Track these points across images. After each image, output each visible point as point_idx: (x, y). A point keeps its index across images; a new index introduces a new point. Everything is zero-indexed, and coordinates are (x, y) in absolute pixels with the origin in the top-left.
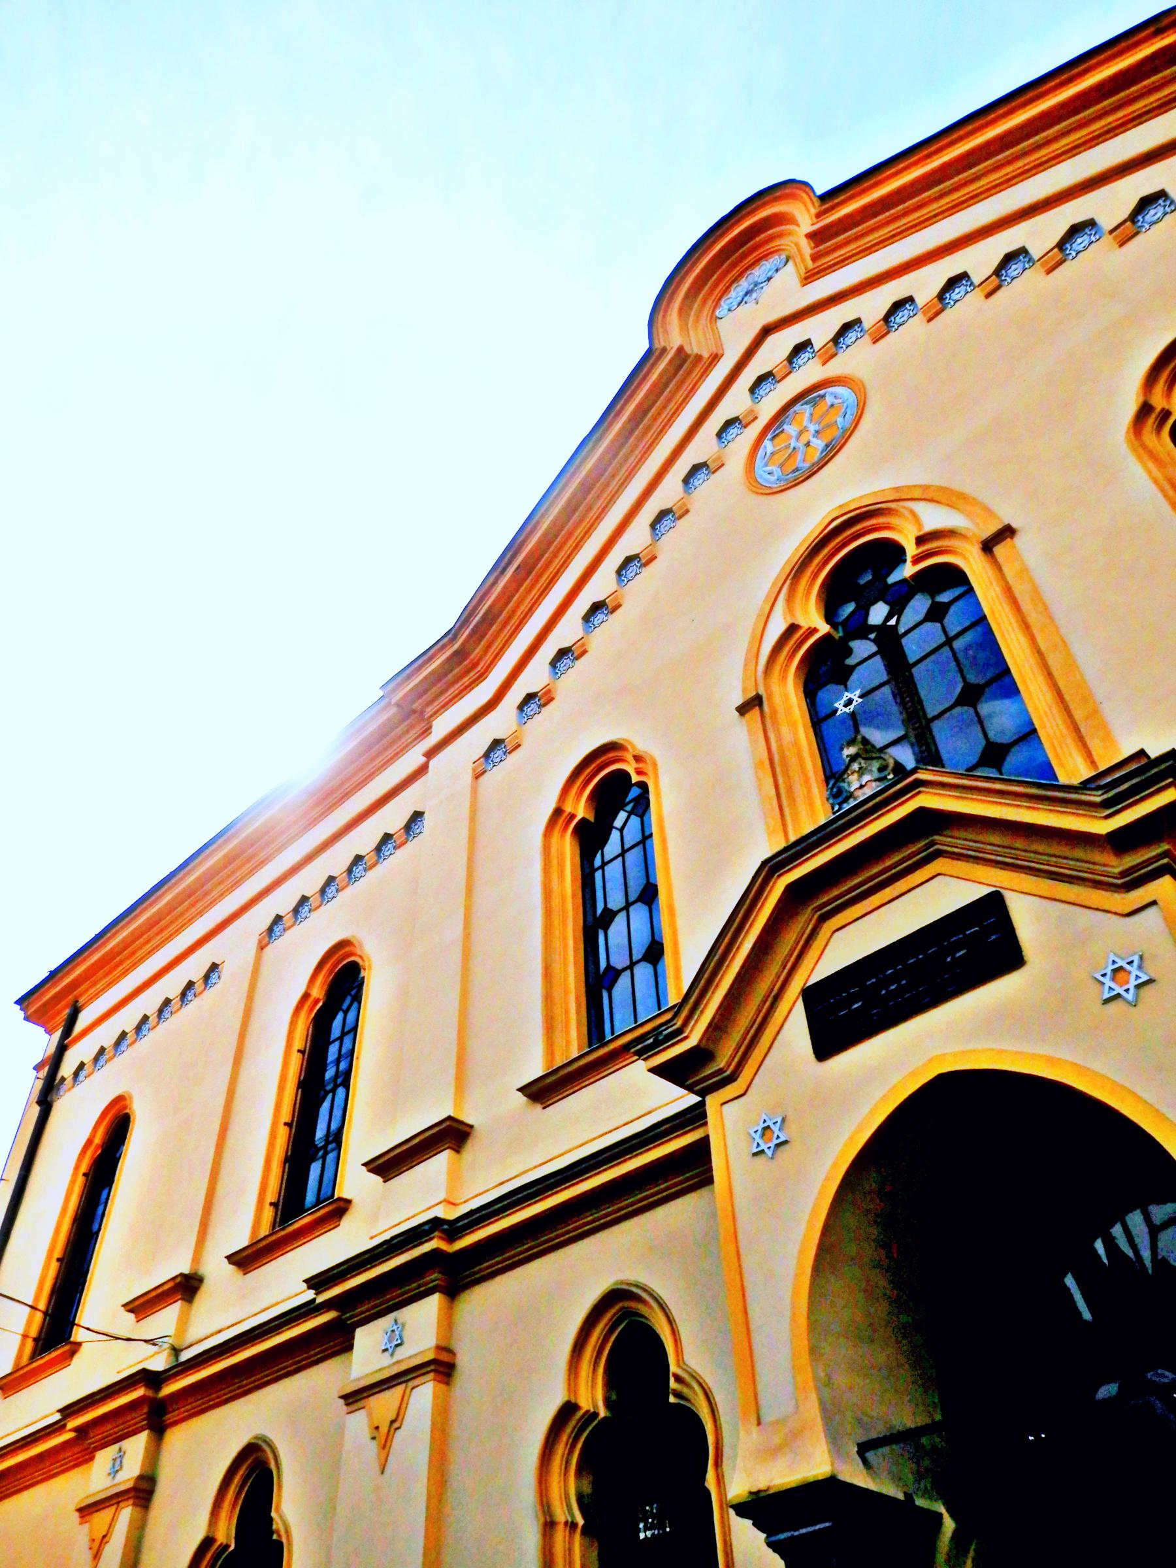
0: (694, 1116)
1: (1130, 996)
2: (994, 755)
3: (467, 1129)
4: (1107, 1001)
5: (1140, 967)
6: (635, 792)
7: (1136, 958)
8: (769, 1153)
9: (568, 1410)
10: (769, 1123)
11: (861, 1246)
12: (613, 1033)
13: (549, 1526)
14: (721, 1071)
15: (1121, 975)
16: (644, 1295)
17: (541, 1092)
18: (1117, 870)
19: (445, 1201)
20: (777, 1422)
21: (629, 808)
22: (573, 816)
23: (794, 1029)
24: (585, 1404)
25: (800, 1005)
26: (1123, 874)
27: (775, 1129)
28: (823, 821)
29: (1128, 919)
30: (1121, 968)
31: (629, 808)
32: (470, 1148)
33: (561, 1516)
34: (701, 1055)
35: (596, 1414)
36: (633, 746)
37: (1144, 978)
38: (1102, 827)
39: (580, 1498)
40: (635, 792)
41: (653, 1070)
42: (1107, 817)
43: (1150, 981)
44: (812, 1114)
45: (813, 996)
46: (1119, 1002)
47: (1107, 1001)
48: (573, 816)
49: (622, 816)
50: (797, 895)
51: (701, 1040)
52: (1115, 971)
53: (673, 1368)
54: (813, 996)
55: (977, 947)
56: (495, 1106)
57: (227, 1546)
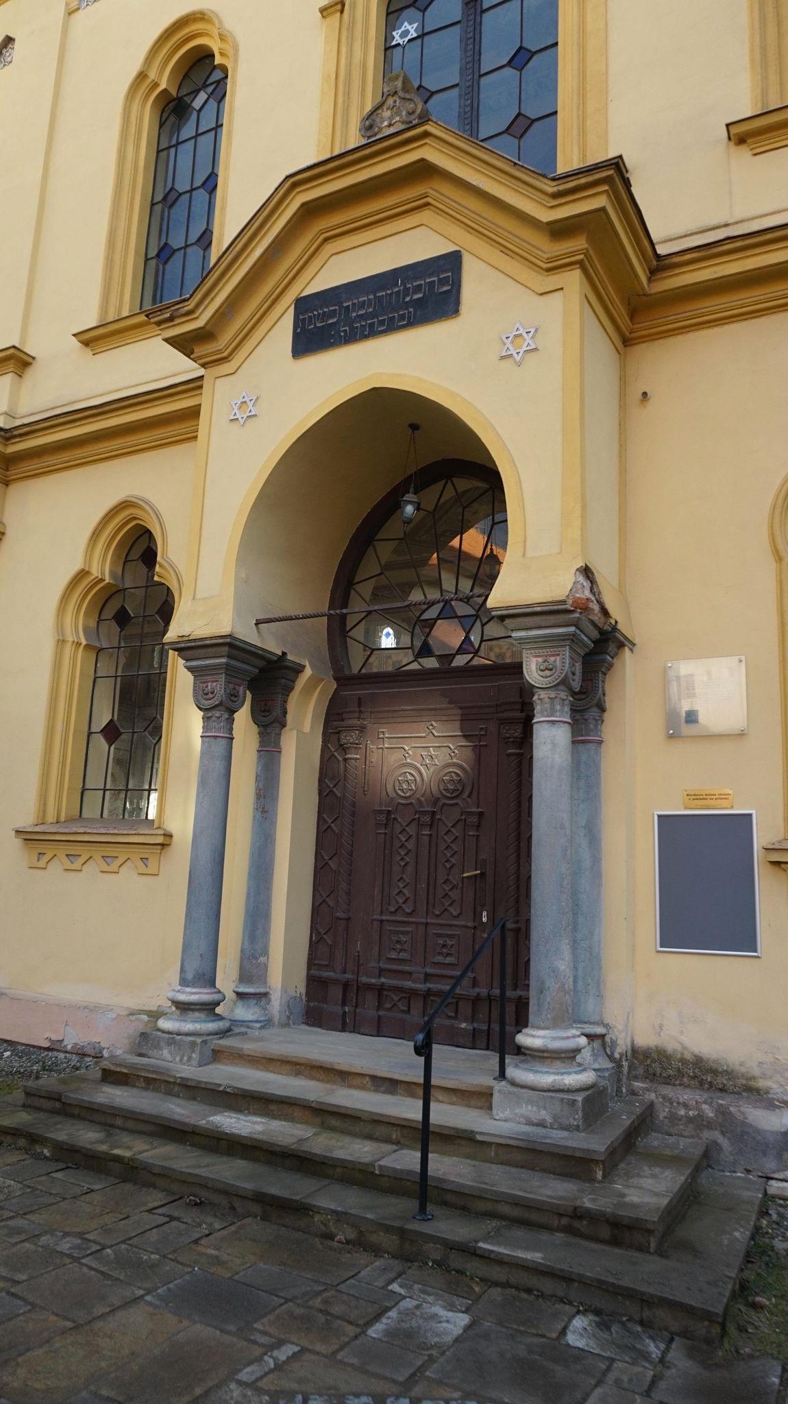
0: (195, 385)
1: (518, 358)
2: (520, 126)
3: (30, 360)
4: (502, 358)
5: (533, 337)
6: (217, 75)
7: (533, 330)
8: (242, 421)
9: (82, 574)
10: (247, 399)
11: (491, 466)
12: (154, 301)
13: (61, 642)
14: (219, 352)
15: (518, 340)
16: (147, 508)
17: (91, 340)
18: (546, 256)
19: (6, 413)
20: (204, 599)
21: (210, 89)
22: (156, 85)
23: (281, 330)
24: (95, 572)
25: (292, 310)
26: (549, 260)
27: (250, 404)
28: (351, 146)
29: (542, 298)
30: (521, 335)
31: (210, 89)
32: (30, 373)
33: (70, 638)
34: (204, 336)
35: (102, 580)
36: (220, 22)
37: (533, 346)
38: (546, 216)
39: (86, 630)
40: (217, 75)
41: (166, 340)
42: (552, 207)
43: (536, 349)
44: (277, 396)
45: (302, 305)
46: (511, 360)
47: (502, 358)
48: (156, 85)
49: (202, 96)
50: (310, 211)
51: (206, 324)
52: (516, 336)
53: (159, 559)
54: (302, 305)
55: (425, 294)
56: (53, 342)
57: (102, 580)
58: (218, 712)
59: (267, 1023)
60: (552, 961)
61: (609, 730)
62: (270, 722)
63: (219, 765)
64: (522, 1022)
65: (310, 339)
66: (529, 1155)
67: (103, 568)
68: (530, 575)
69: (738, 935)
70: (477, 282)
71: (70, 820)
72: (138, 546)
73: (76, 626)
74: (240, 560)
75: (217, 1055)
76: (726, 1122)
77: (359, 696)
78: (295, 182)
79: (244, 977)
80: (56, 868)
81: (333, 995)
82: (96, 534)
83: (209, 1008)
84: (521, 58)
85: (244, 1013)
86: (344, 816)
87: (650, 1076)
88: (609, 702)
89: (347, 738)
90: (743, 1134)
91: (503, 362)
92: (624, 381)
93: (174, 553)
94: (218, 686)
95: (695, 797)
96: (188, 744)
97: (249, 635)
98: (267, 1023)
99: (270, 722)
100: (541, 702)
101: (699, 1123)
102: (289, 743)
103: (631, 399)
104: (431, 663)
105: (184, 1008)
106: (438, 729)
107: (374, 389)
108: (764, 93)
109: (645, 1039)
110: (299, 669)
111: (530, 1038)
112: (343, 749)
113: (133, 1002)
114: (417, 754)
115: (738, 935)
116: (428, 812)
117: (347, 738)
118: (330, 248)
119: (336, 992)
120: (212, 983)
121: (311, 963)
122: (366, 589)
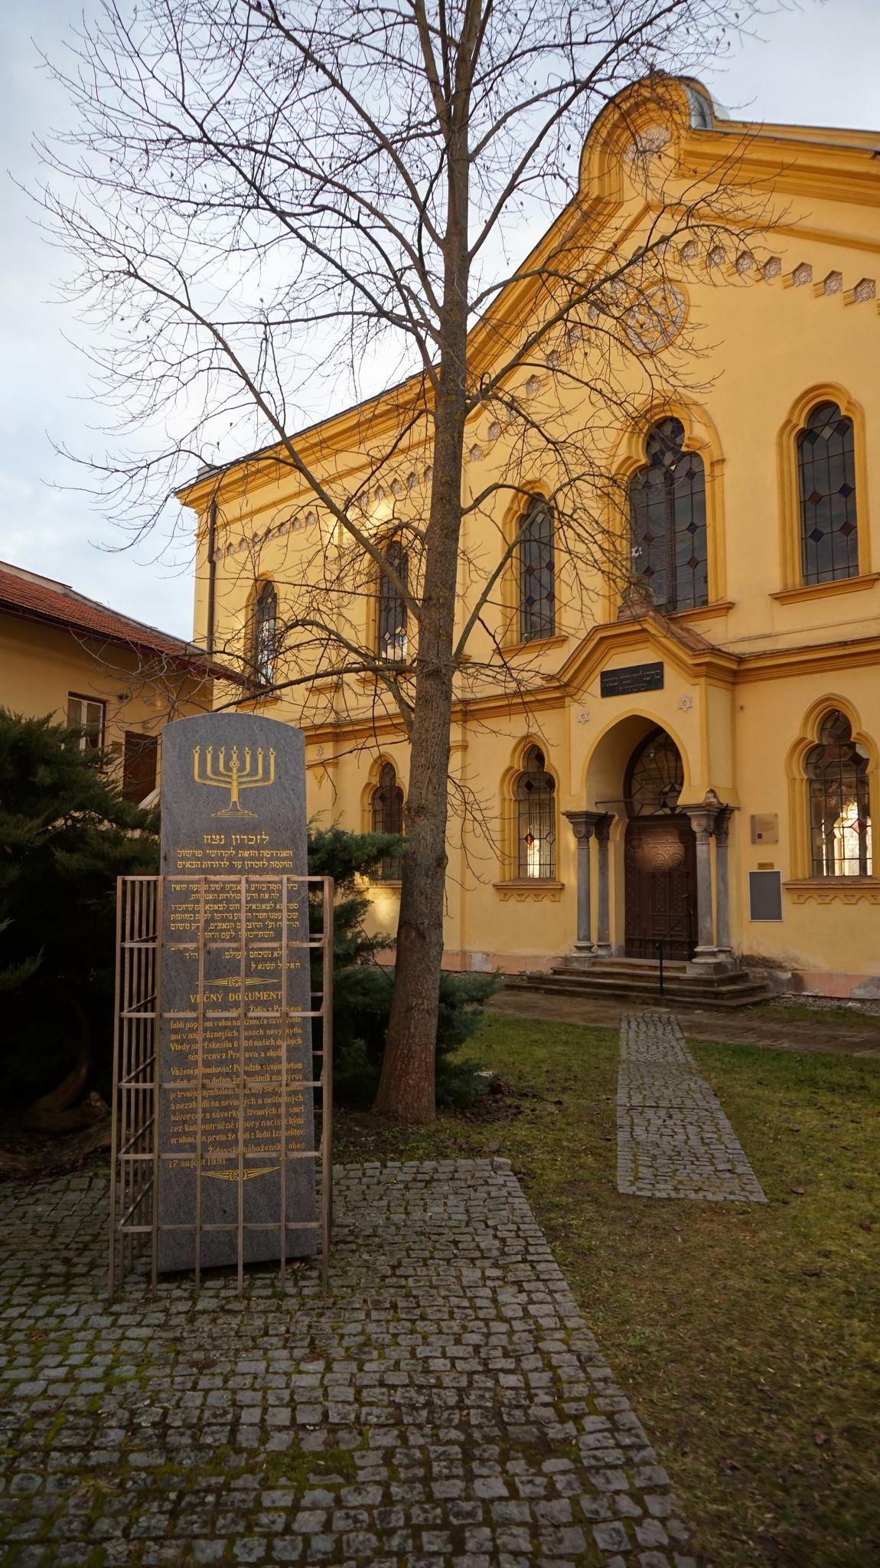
13: (504, 799)
23: (595, 686)
45: (604, 675)
54: (604, 675)
55: (649, 678)
58: (583, 839)
59: (610, 956)
60: (708, 924)
61: (730, 842)
62: (603, 839)
63: (585, 859)
64: (696, 944)
65: (608, 691)
66: (696, 981)
67: (519, 765)
68: (691, 795)
69: (776, 914)
70: (670, 674)
71: (516, 879)
72: (535, 754)
73: (509, 791)
74: (587, 780)
75: (594, 964)
76: (771, 977)
77: (638, 829)
78: (597, 629)
79: (600, 940)
80: (530, 900)
81: (634, 945)
82: (515, 750)
83: (589, 948)
84: (692, 528)
85: (602, 952)
86: (634, 871)
87: (749, 965)
88: (730, 831)
89: (636, 843)
90: (777, 982)
91: (679, 708)
92: (733, 700)
93: (554, 760)
94: (583, 829)
95: (761, 866)
96: (568, 848)
97: (594, 810)
98: (610, 956)
99: (603, 839)
100: (698, 835)
101: (763, 978)
102: (611, 847)
103: (736, 709)
104: (668, 811)
105: (579, 948)
106: (670, 839)
107: (634, 716)
108: (785, 577)
109: (746, 953)
110: (613, 817)
111: (698, 949)
112: (633, 847)
113: (553, 953)
114: (663, 851)
115: (776, 914)
116: (669, 874)
117: (636, 843)
118: (612, 652)
119: (637, 944)
120: (589, 940)
121: (626, 933)
122: (638, 777)
